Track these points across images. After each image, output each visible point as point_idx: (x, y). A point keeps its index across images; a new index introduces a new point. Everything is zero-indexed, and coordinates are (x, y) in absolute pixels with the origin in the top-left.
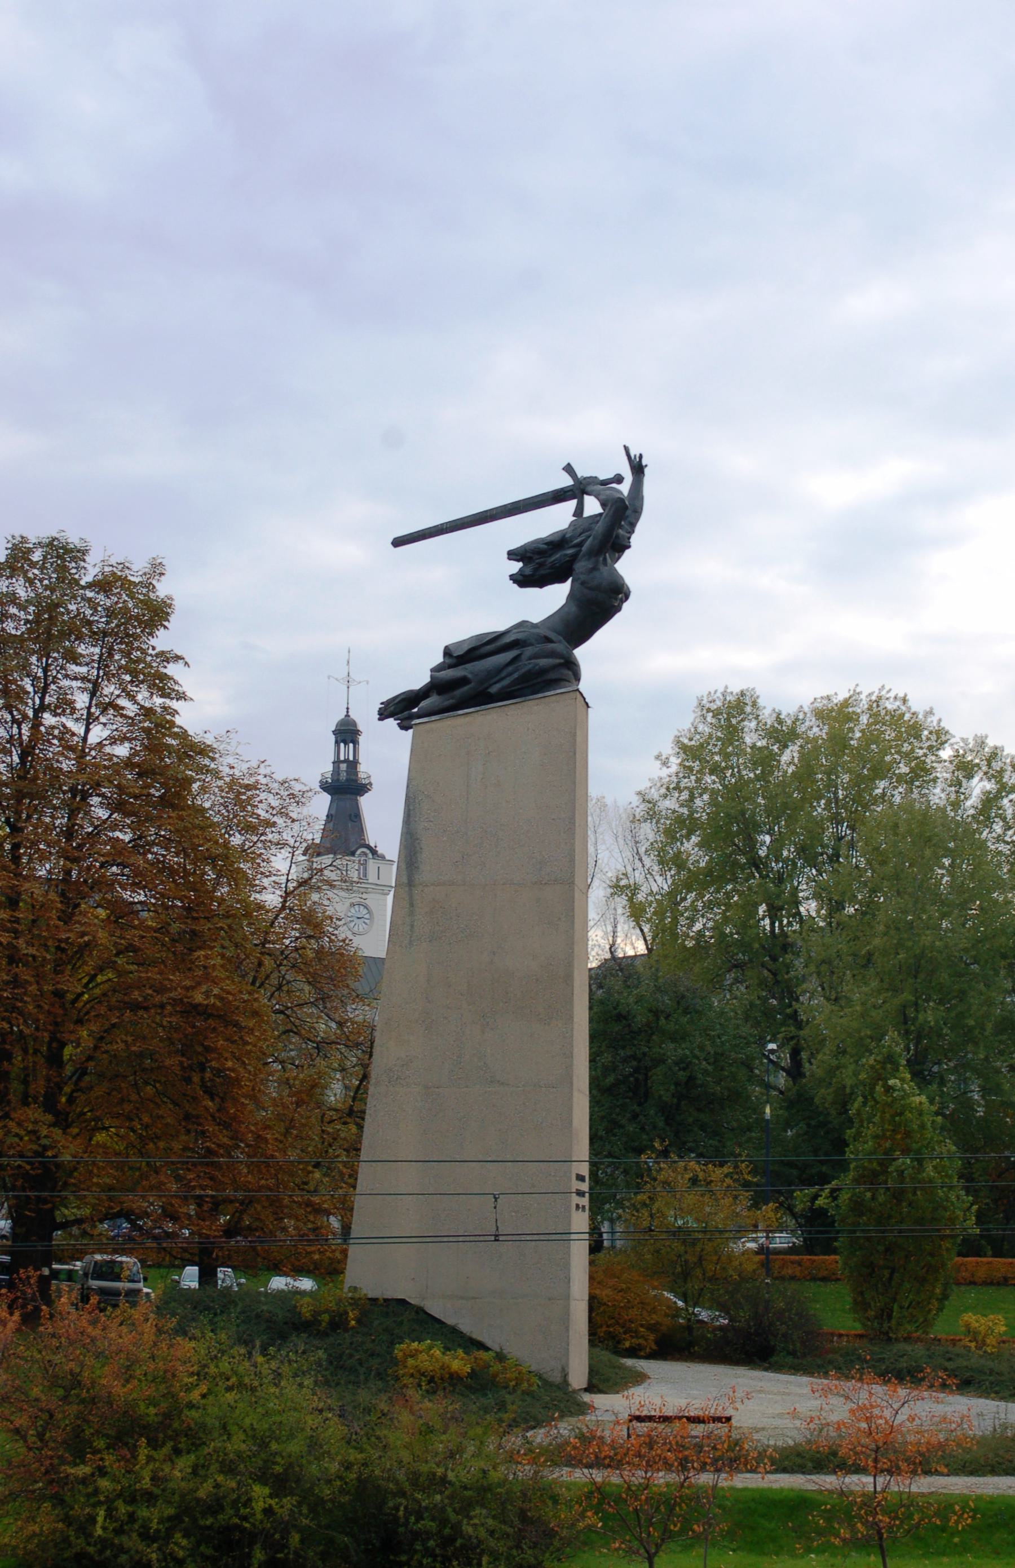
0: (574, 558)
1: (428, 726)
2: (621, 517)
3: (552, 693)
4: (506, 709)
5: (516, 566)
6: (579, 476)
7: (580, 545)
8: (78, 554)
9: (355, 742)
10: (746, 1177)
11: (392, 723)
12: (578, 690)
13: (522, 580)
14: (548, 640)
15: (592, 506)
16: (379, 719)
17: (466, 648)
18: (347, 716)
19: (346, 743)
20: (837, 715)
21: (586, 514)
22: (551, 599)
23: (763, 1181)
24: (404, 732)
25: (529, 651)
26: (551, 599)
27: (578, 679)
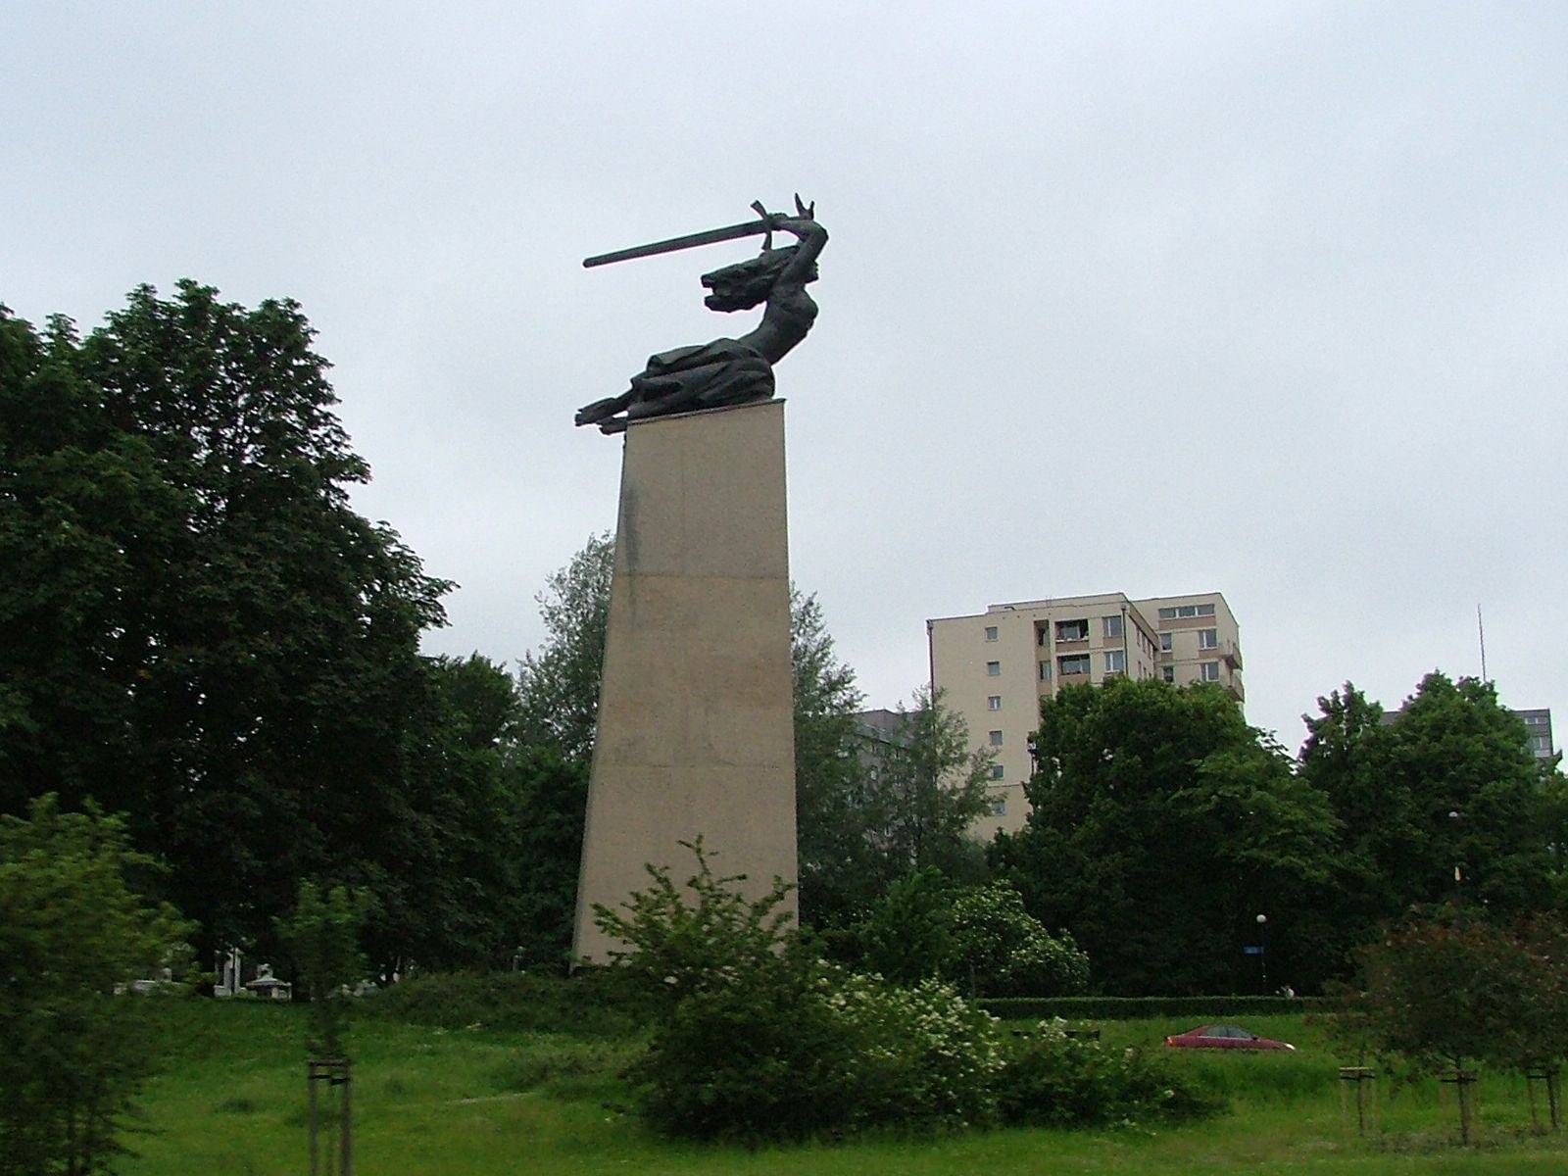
0: (771, 284)
3: (761, 402)
4: (719, 414)
6: (768, 212)
7: (779, 271)
8: (329, 399)
14: (753, 354)
15: (783, 240)
17: (675, 357)
24: (606, 436)
25: (737, 363)
26: (745, 323)
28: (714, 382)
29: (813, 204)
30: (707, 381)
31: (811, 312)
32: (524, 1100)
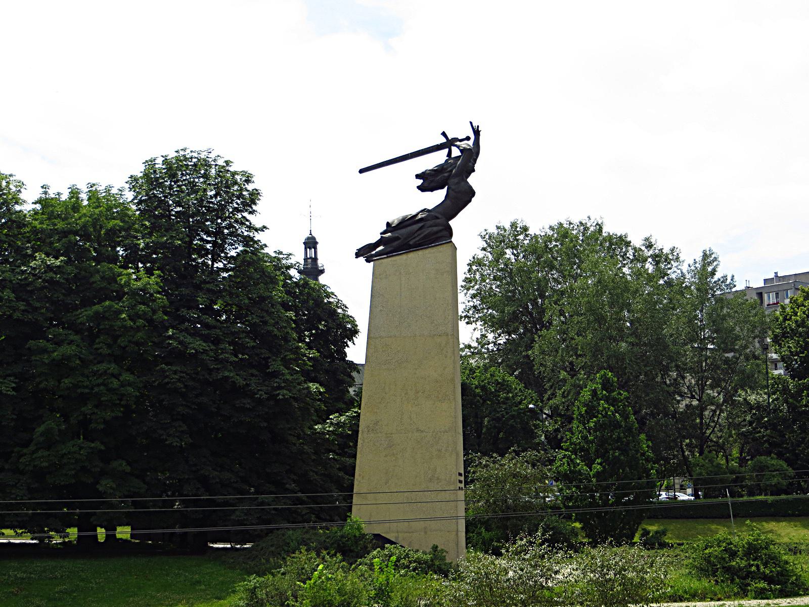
0: (449, 177)
1: (380, 261)
2: (471, 155)
5: (420, 182)
6: (450, 139)
9: (315, 248)
10: (175, 210)
11: (362, 259)
12: (451, 242)
13: (422, 188)
14: (437, 218)
15: (456, 152)
16: (356, 258)
18: (311, 234)
19: (310, 249)
20: (563, 232)
21: (453, 156)
22: (437, 197)
23: (590, 540)
25: (429, 223)
26: (437, 197)
27: (451, 235)
28: (416, 235)
29: (311, 243)
30: (411, 235)
31: (472, 193)
32: (234, 382)
